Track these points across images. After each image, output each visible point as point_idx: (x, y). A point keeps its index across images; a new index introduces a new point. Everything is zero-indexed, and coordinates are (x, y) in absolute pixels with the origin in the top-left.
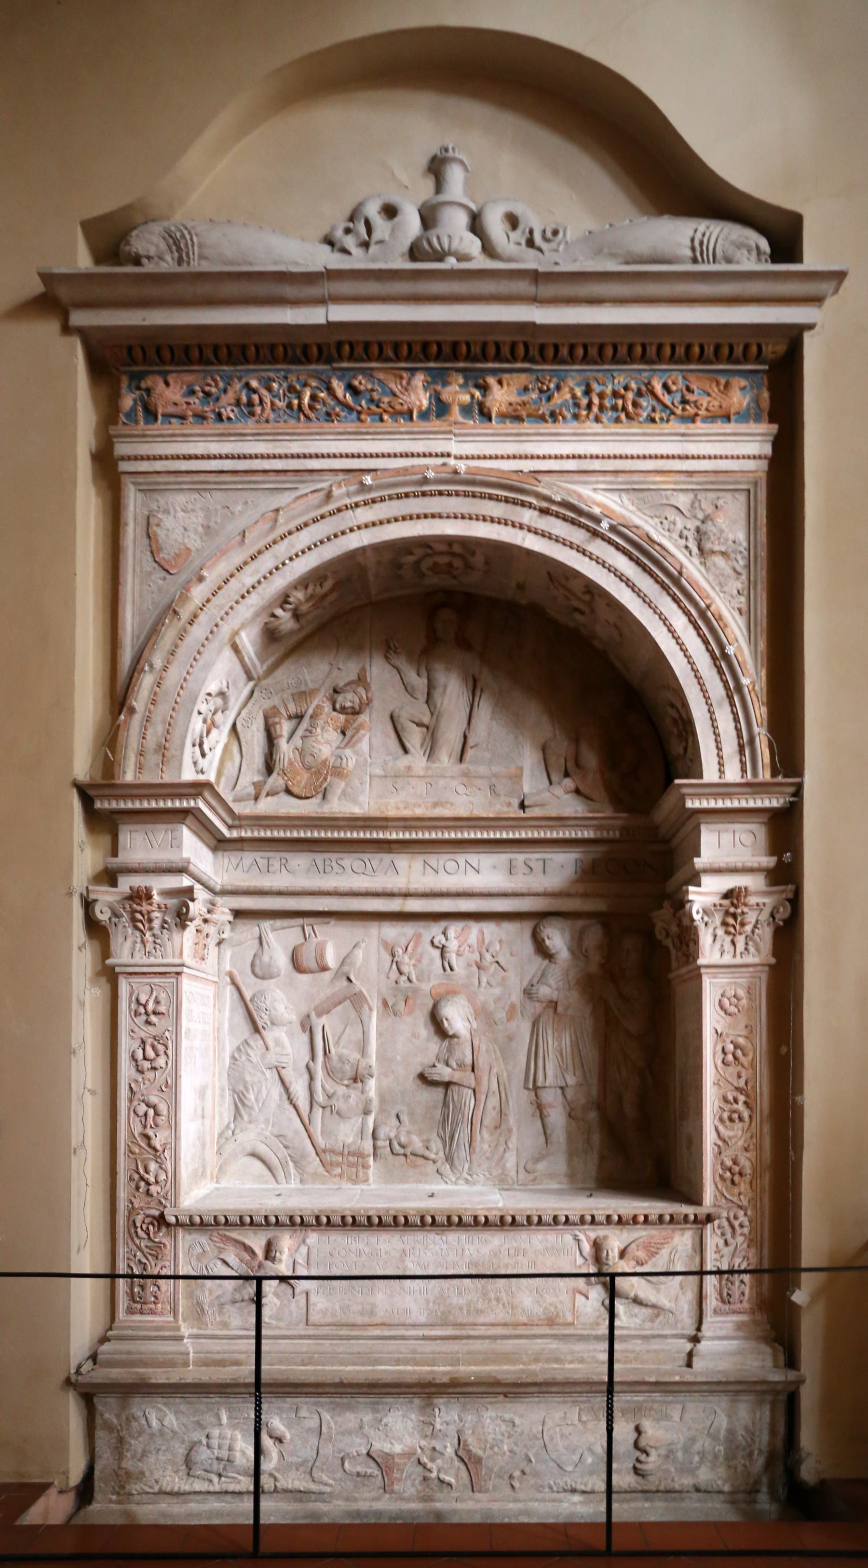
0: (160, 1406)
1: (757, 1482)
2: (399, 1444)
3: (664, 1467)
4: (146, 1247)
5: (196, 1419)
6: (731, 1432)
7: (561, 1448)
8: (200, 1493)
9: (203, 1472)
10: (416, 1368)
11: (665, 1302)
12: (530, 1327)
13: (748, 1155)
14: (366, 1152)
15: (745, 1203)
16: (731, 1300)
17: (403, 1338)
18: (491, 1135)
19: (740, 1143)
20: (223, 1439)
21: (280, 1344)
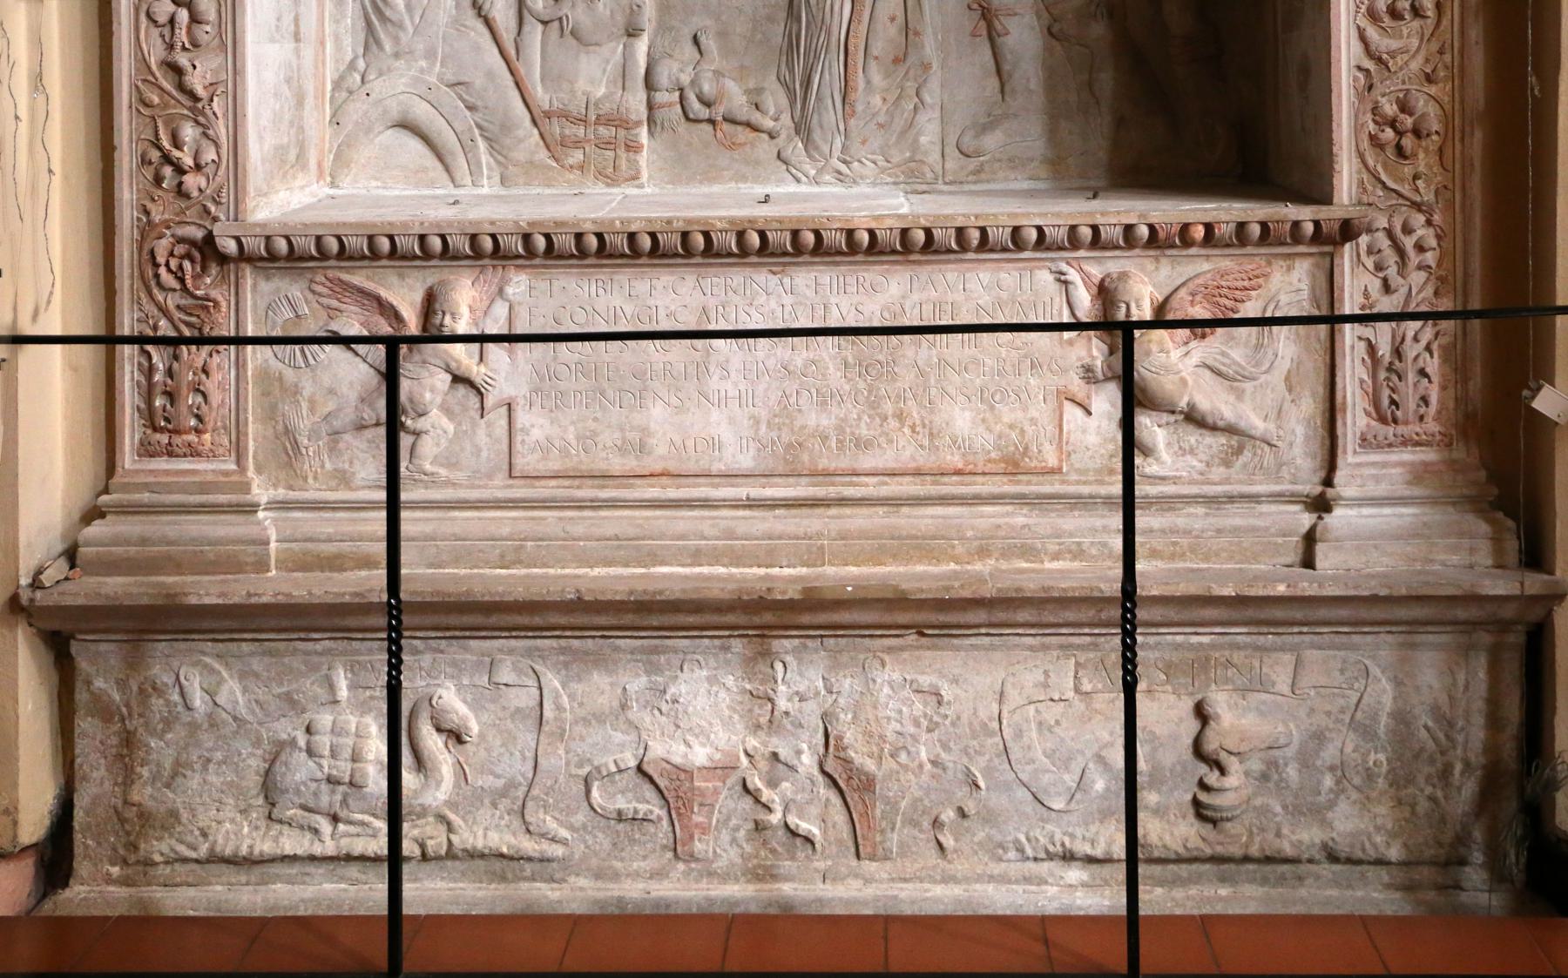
0: (208, 660)
1: (1462, 839)
2: (703, 745)
3: (1258, 802)
4: (178, 307)
5: (284, 689)
6: (1402, 718)
7: (1039, 755)
8: (293, 859)
9: (300, 812)
10: (734, 570)
11: (1256, 422)
12: (968, 479)
13: (1433, 90)
14: (633, 117)
15: (1429, 197)
16: (1399, 414)
17: (706, 504)
18: (887, 75)
19: (1415, 65)
20: (339, 735)
21: (455, 519)
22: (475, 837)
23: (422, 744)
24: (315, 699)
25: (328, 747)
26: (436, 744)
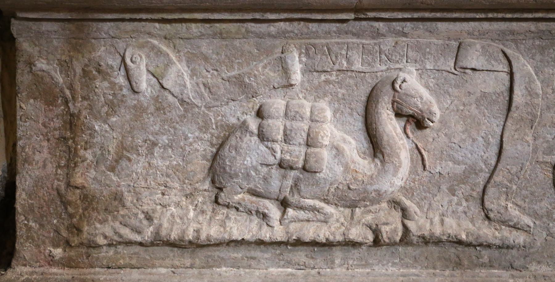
9: (248, 197)
20: (294, 119)
22: (432, 223)
23: (381, 129)
24: (267, 82)
25: (281, 132)
26: (395, 128)
